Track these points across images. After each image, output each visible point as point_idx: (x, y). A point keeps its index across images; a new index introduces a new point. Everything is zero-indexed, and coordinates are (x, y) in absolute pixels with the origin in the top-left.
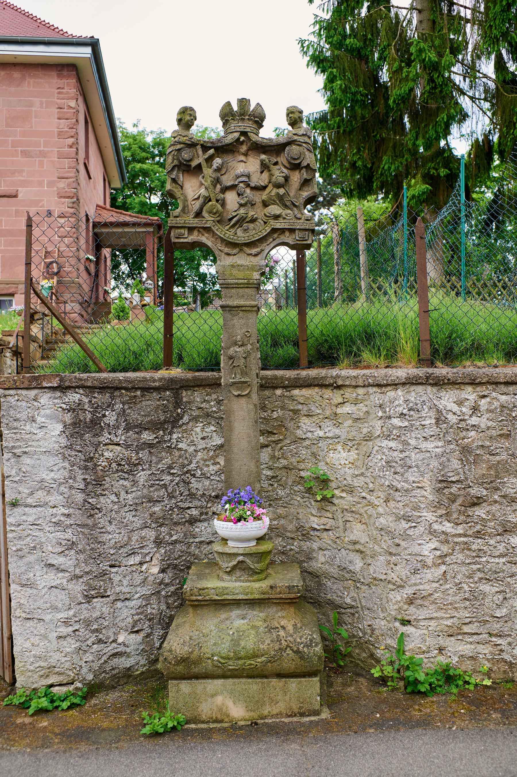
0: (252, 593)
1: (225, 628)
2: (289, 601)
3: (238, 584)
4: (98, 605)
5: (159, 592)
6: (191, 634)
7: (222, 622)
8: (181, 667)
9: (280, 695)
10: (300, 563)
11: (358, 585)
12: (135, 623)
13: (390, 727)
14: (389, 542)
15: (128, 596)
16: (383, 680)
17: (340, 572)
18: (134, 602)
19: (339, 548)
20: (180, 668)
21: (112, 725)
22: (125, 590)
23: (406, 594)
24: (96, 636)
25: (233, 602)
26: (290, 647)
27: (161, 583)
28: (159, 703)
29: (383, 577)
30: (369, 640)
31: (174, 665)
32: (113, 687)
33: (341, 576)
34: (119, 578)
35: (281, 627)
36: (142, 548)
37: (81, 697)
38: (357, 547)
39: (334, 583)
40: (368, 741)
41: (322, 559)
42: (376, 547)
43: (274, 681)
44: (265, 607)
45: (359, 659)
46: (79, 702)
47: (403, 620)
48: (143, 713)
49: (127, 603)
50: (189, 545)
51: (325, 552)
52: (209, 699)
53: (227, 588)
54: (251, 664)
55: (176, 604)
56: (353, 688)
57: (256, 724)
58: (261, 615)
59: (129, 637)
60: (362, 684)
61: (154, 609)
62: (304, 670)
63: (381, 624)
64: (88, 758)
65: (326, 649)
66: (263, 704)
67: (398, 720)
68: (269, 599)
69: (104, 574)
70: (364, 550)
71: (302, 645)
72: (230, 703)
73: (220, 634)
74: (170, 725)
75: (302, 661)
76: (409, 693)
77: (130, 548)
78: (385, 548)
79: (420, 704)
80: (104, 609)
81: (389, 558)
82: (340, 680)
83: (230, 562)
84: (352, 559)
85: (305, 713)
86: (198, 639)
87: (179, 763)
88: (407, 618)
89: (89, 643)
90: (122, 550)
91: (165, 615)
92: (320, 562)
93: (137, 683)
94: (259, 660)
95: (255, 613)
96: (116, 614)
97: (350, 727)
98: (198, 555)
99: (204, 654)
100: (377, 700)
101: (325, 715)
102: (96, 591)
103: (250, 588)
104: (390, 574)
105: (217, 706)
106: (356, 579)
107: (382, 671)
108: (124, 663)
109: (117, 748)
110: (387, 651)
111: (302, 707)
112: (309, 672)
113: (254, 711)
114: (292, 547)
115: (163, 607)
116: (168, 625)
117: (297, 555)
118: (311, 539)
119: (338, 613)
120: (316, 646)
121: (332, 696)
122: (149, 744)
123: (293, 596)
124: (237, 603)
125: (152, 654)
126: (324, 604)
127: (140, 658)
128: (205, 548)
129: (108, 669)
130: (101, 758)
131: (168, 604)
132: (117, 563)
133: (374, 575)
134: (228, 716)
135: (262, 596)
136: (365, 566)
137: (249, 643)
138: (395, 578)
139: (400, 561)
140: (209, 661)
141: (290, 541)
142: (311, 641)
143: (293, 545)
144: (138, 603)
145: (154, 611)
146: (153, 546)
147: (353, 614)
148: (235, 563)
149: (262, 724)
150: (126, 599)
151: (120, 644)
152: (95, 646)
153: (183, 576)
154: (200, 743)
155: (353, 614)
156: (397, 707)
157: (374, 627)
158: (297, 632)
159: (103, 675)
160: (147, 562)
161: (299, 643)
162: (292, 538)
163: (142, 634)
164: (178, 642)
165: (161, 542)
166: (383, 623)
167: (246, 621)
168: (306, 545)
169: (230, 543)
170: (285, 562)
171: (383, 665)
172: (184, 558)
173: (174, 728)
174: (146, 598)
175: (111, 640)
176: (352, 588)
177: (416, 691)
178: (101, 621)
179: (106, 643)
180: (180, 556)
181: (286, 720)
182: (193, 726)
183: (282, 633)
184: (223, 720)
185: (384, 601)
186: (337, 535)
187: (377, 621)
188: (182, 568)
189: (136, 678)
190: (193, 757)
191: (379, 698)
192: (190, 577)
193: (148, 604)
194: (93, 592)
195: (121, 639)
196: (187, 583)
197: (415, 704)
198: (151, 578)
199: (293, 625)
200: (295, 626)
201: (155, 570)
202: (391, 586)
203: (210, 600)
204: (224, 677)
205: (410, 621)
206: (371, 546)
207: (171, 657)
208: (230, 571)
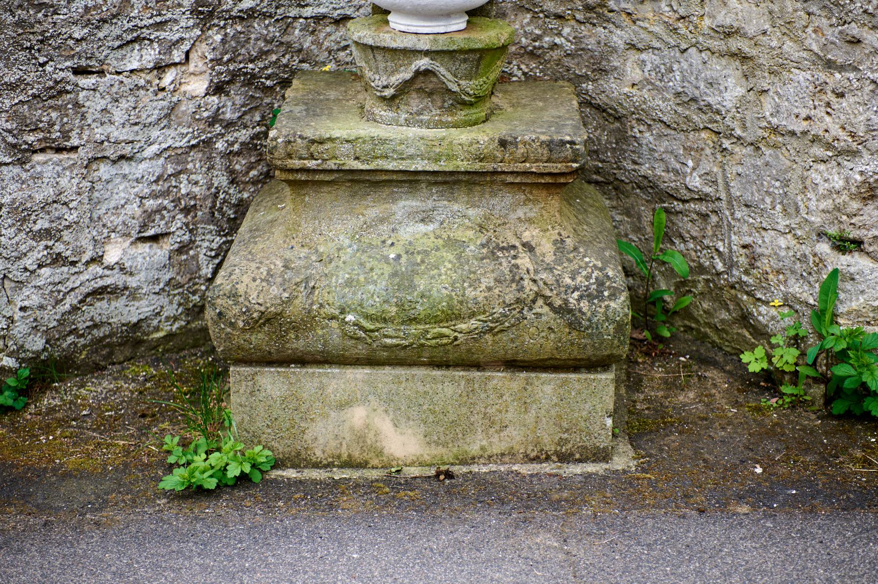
0: (450, 158)
1: (376, 242)
2: (549, 180)
3: (414, 132)
4: (48, 171)
5: (208, 143)
6: (288, 255)
7: (368, 226)
8: (260, 336)
9: (511, 409)
10: (577, 80)
11: (726, 144)
12: (149, 217)
13: (791, 503)
14: (829, 32)
15: (127, 150)
16: (770, 380)
17: (680, 109)
18: (143, 166)
19: (684, 46)
20: (259, 339)
21: (88, 465)
22: (116, 134)
23: (862, 173)
24: (47, 247)
25: (400, 177)
26: (546, 298)
27: (214, 120)
28: (209, 412)
29: (799, 126)
30: (740, 282)
31: (243, 330)
32: (97, 369)
33: (681, 120)
34: (101, 104)
35: (524, 245)
36: (160, 26)
37: (15, 389)
38: (735, 44)
39: (660, 136)
40: (734, 535)
41: (634, 73)
42: (789, 46)
43: (499, 378)
44: (482, 195)
45: (708, 325)
46: (10, 402)
47: (843, 239)
48: (168, 439)
49: (126, 168)
50: (287, 24)
51: (644, 56)
52: (333, 414)
53: (384, 141)
54: (442, 336)
55: (253, 173)
56: (691, 395)
57: (449, 475)
58: (471, 212)
59: (133, 251)
60: (715, 385)
61: (196, 183)
62: (575, 354)
63: (777, 245)
64: (21, 551)
65: (635, 301)
66: (470, 429)
67: (811, 484)
68: (495, 173)
69: (58, 90)
70: (754, 52)
71: (576, 295)
72: (384, 425)
73: (364, 258)
74: (233, 471)
75: (575, 334)
76: (838, 417)
77: (127, 26)
78: (815, 48)
79: (867, 446)
80: (64, 182)
81: (822, 76)
82: (658, 373)
83: (393, 73)
84: (715, 74)
85: (572, 455)
86: (307, 268)
87: (251, 571)
88: (854, 234)
89: (29, 262)
90: (106, 30)
91: (225, 201)
92: (628, 80)
93: (158, 360)
94: (463, 326)
95: (456, 207)
96: (96, 194)
97: (686, 496)
98: (309, 51)
99: (321, 306)
100: (755, 428)
101: (624, 460)
102: (41, 135)
103: (445, 143)
104: (821, 120)
105: (352, 429)
106: (721, 129)
107: (769, 357)
108: (122, 312)
109: (97, 524)
110: (786, 310)
111: (567, 441)
112: (589, 359)
113: (445, 445)
114: (557, 40)
115: (221, 180)
116: (234, 225)
117: (568, 62)
118: (608, 21)
119: (667, 211)
120: (613, 296)
121: (639, 414)
122: (178, 517)
123: (559, 167)
124: (410, 180)
125: (194, 293)
126: (629, 187)
127: (163, 300)
128: (329, 34)
129: (81, 326)
130: (54, 550)
131: (232, 172)
132: (93, 63)
133: (775, 121)
134: (380, 453)
135: (477, 166)
136: (751, 96)
137: (438, 284)
138: (836, 130)
139: (856, 84)
140: (334, 324)
141: (554, 24)
142: (600, 283)
143: (559, 34)
144: (156, 167)
145: (196, 190)
146: (191, 23)
147: (705, 217)
148: (408, 76)
149: (464, 475)
150: (122, 157)
151: (110, 268)
152: (45, 271)
153: (270, 106)
154: (308, 519)
155: (705, 217)
156: (807, 451)
157: (759, 251)
158: (567, 261)
159: (71, 339)
160: (175, 64)
161: (568, 287)
162: (559, 17)
163: (167, 246)
164: (255, 273)
165: (211, 14)
166: (782, 242)
167: (431, 227)
168: (595, 36)
169: (396, 22)
170: (535, 79)
171: (773, 347)
172: (274, 57)
173: (243, 479)
174: (179, 156)
175: (86, 257)
176: (708, 151)
177: (858, 412)
178: (58, 210)
179: (73, 263)
180: (263, 54)
181: (525, 469)
182: (291, 473)
183: (525, 261)
184: (367, 463)
185: (794, 188)
186: (682, 12)
187: (768, 236)
188: (268, 83)
189: (155, 348)
190: (289, 558)
191: (760, 424)
192: (286, 108)
193: (180, 173)
194: (31, 138)
195: (112, 255)
196: (277, 125)
197: (854, 445)
198: (187, 107)
199: (555, 242)
200: (559, 243)
201: (198, 86)
202: (818, 151)
203: (338, 171)
204: (371, 362)
205: (862, 242)
206: (774, 44)
207: (236, 310)
208: (393, 97)
